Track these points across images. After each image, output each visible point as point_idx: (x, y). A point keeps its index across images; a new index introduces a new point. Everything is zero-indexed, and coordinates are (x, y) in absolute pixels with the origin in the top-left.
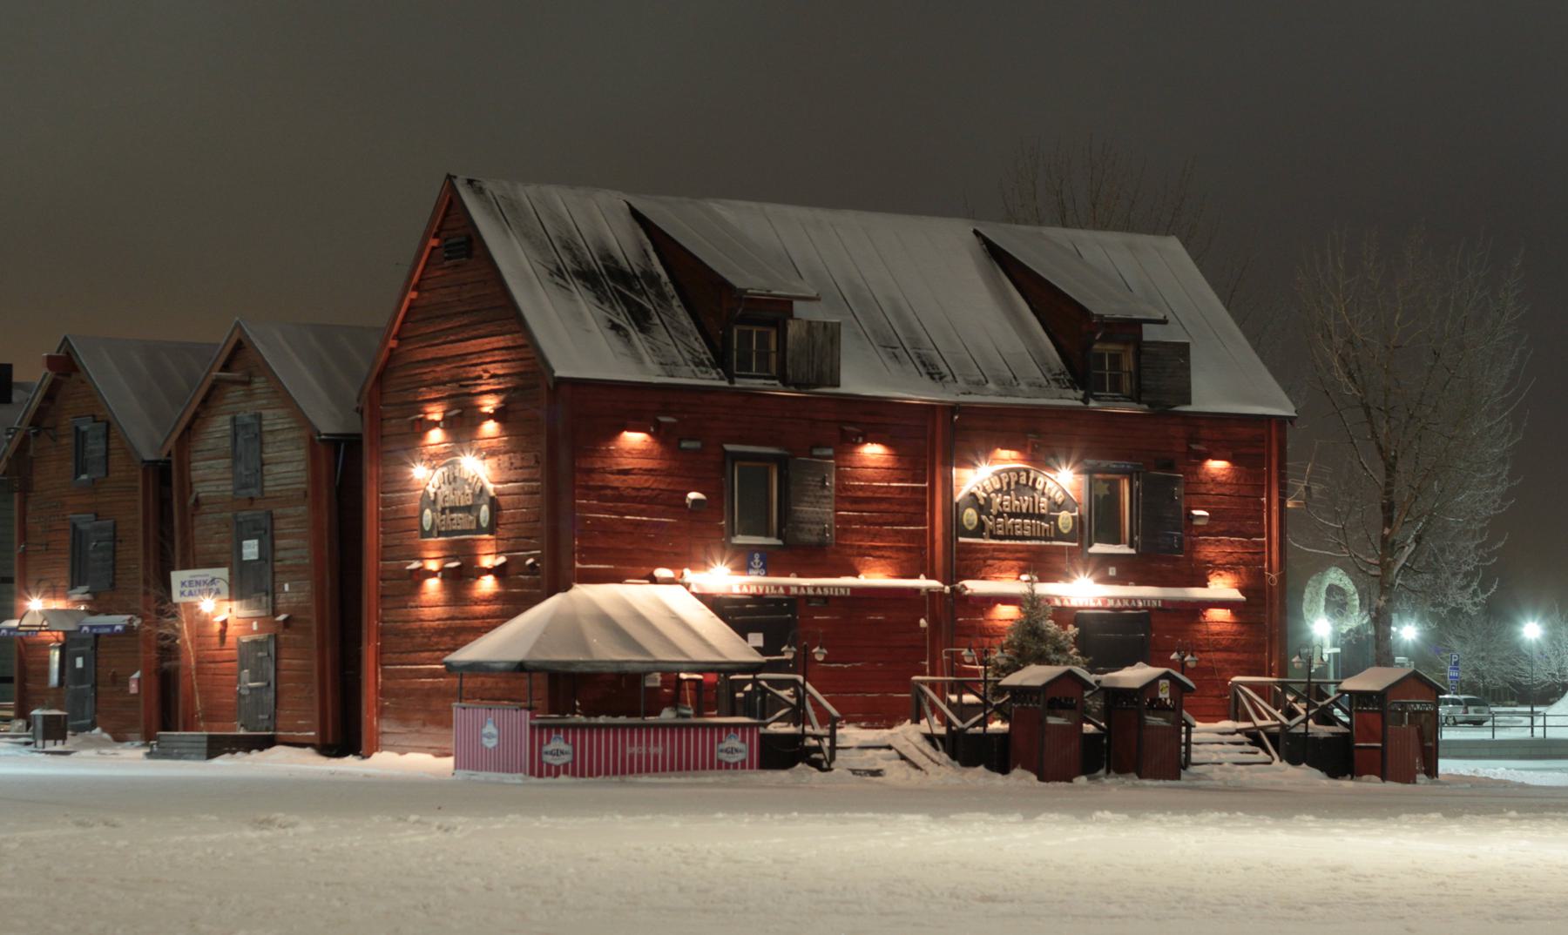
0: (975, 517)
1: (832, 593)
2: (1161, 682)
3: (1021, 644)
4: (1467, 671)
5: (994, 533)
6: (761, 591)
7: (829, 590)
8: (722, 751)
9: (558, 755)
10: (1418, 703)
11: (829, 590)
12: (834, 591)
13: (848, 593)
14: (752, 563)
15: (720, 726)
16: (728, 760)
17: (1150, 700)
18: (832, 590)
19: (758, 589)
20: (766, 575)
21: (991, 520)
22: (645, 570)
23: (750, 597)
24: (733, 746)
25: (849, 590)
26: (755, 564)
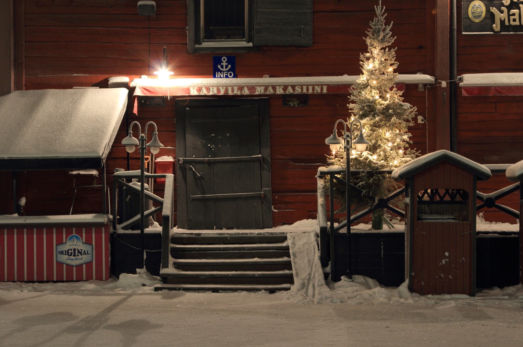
0: (484, 9)
1: (305, 91)
2: (124, 141)
3: (370, 125)
4: (393, 62)
5: (507, 23)
6: (222, 93)
7: (302, 89)
8: (62, 253)
9: (75, 255)
10: (146, 144)
11: (302, 89)
12: (308, 89)
13: (325, 91)
14: (219, 66)
15: (59, 226)
16: (69, 262)
17: (432, 191)
18: (305, 88)
19: (219, 90)
20: (235, 76)
21: (502, 12)
22: (101, 77)
23: (74, 87)
24: (76, 247)
25: (325, 88)
26: (222, 67)
